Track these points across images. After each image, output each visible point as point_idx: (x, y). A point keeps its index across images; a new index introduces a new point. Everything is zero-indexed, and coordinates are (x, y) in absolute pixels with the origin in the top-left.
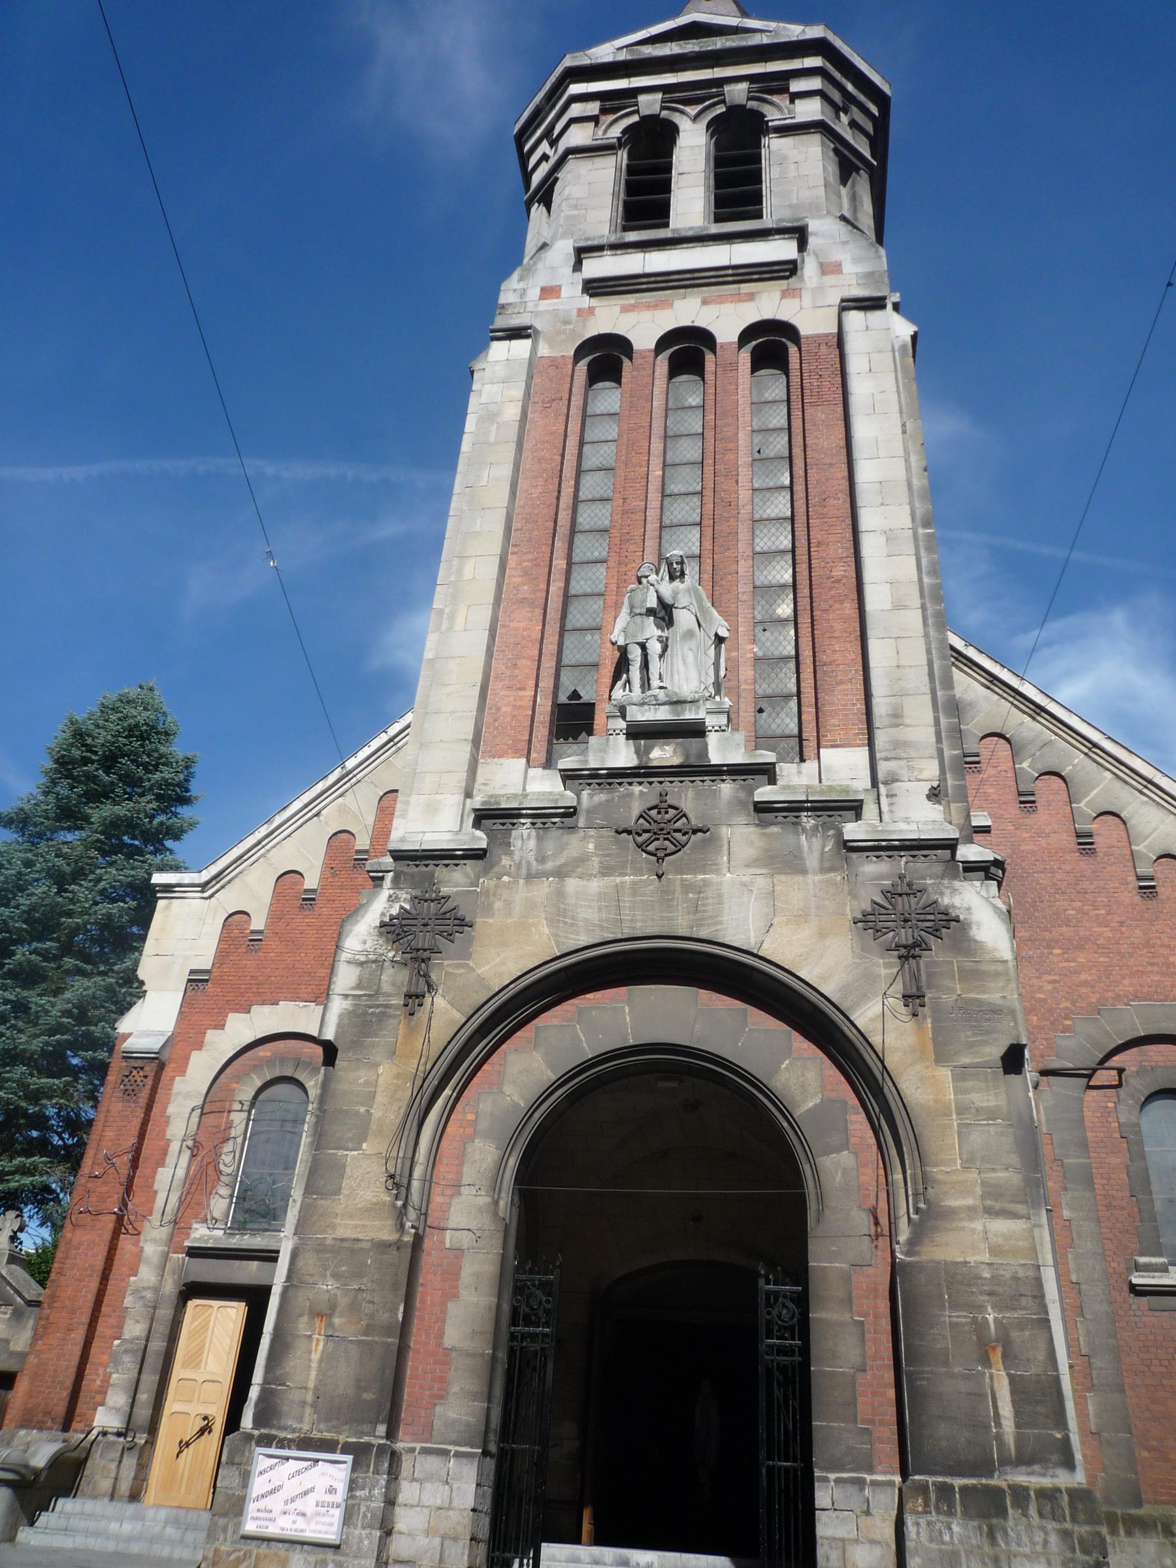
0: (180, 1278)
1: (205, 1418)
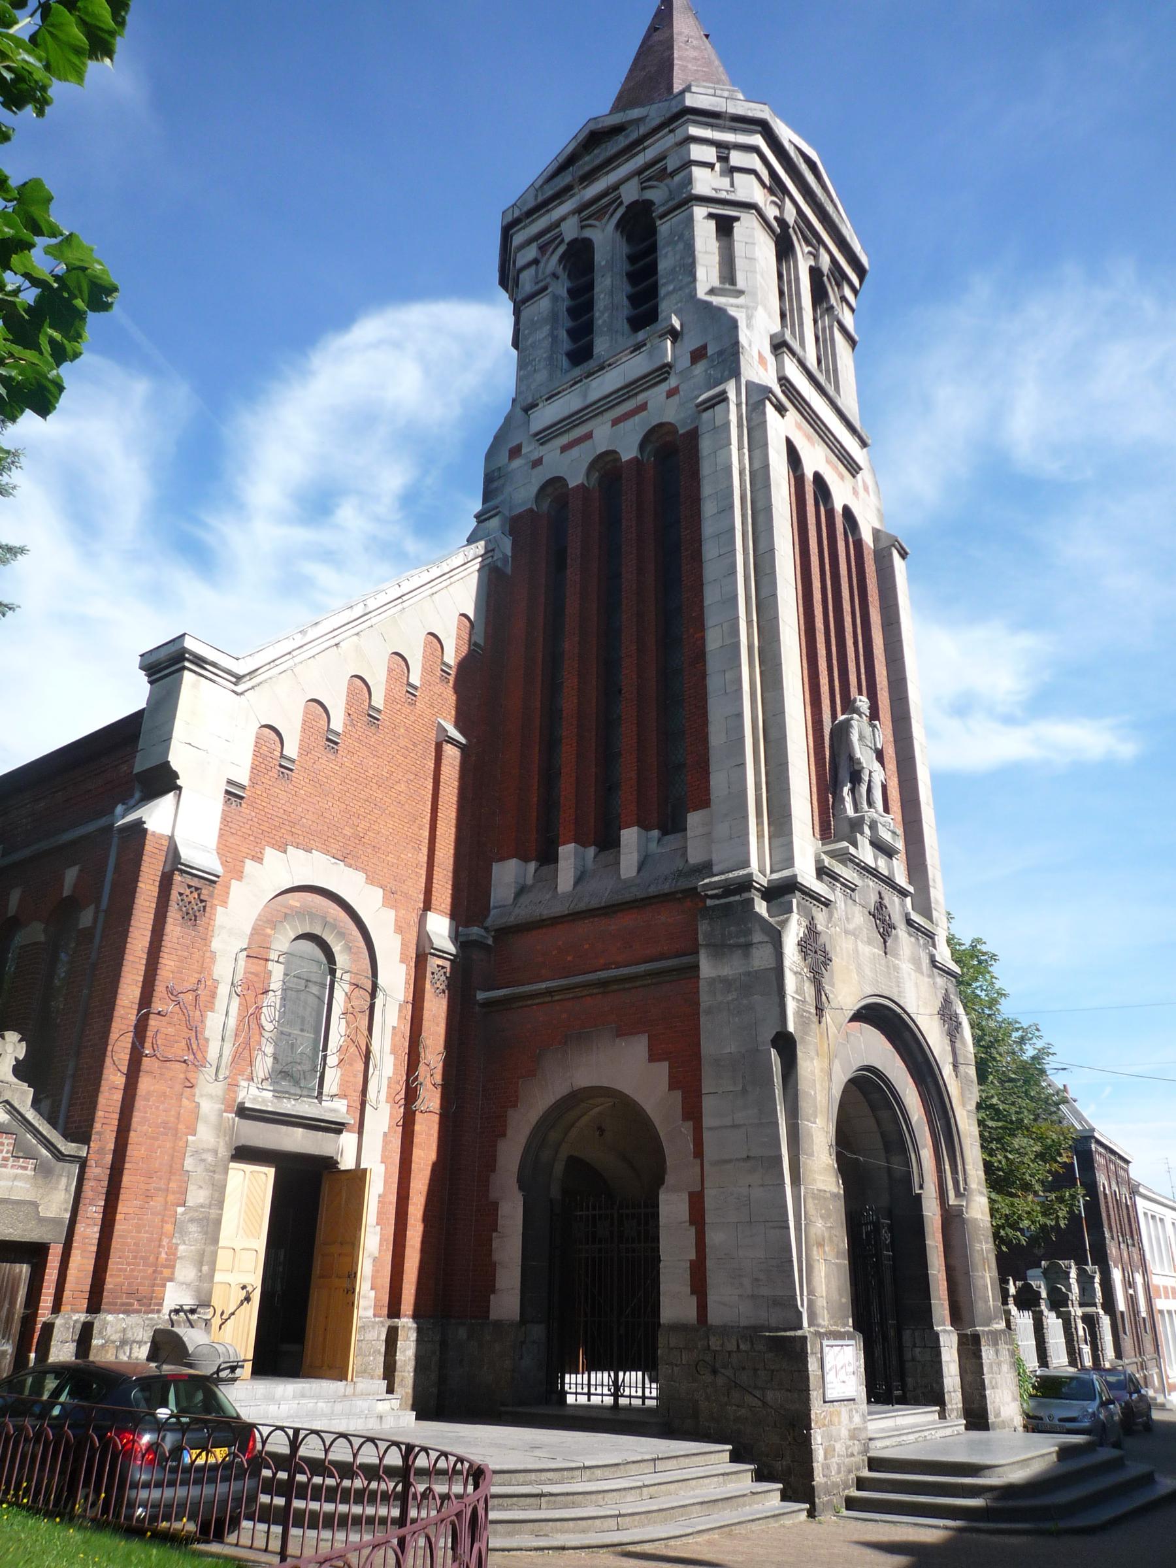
0: (231, 1139)
1: (244, 1288)
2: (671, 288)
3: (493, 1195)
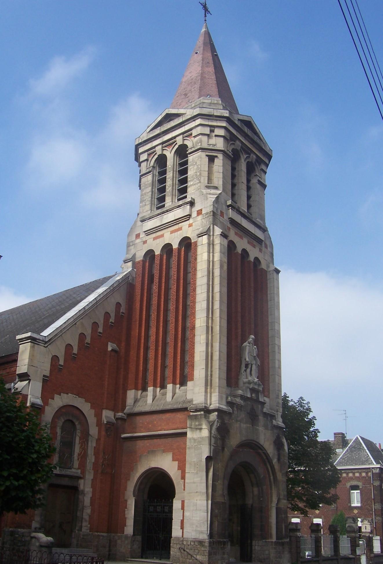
2: (192, 183)
3: (126, 498)
